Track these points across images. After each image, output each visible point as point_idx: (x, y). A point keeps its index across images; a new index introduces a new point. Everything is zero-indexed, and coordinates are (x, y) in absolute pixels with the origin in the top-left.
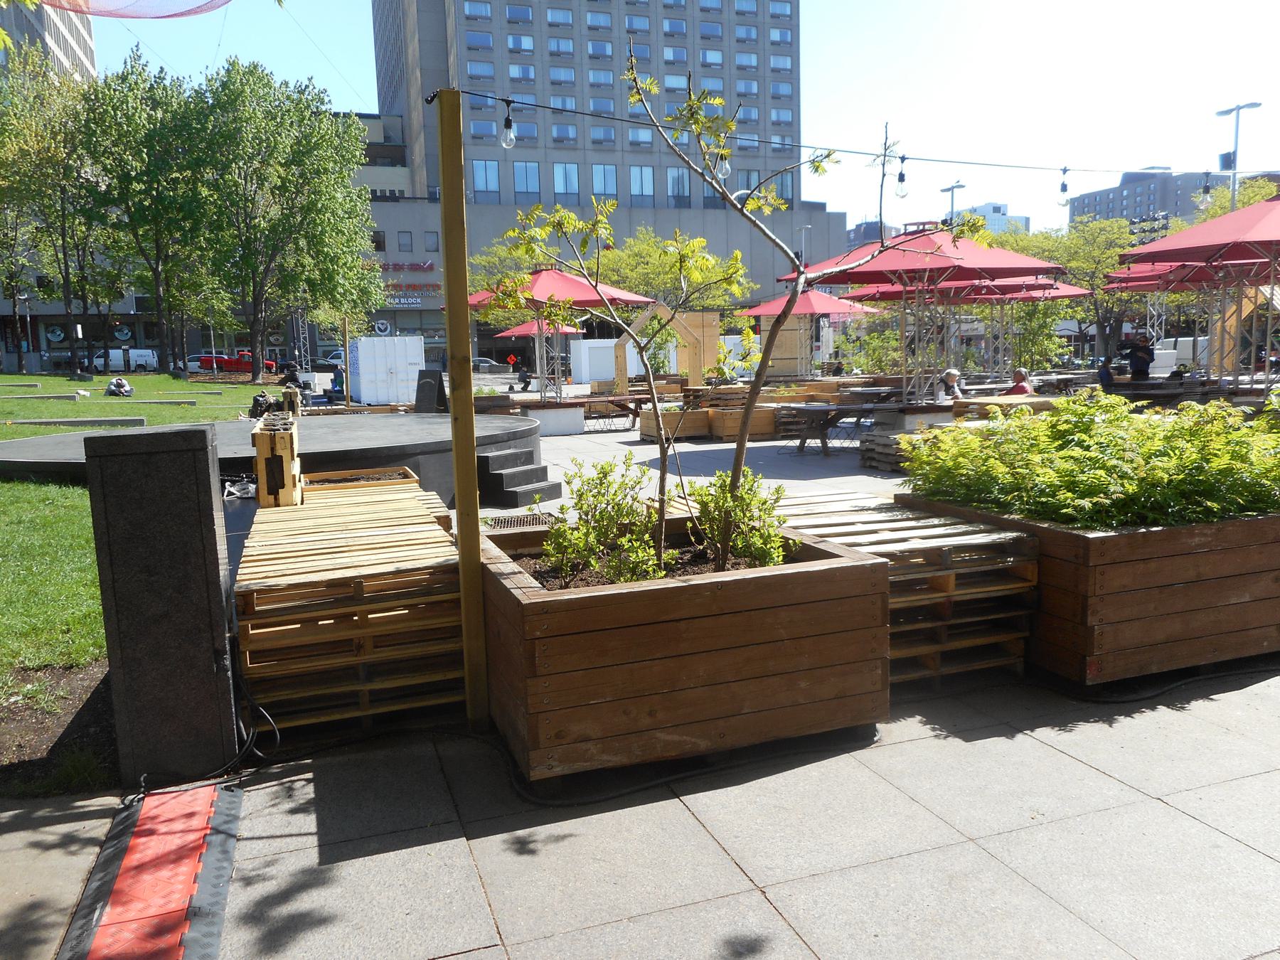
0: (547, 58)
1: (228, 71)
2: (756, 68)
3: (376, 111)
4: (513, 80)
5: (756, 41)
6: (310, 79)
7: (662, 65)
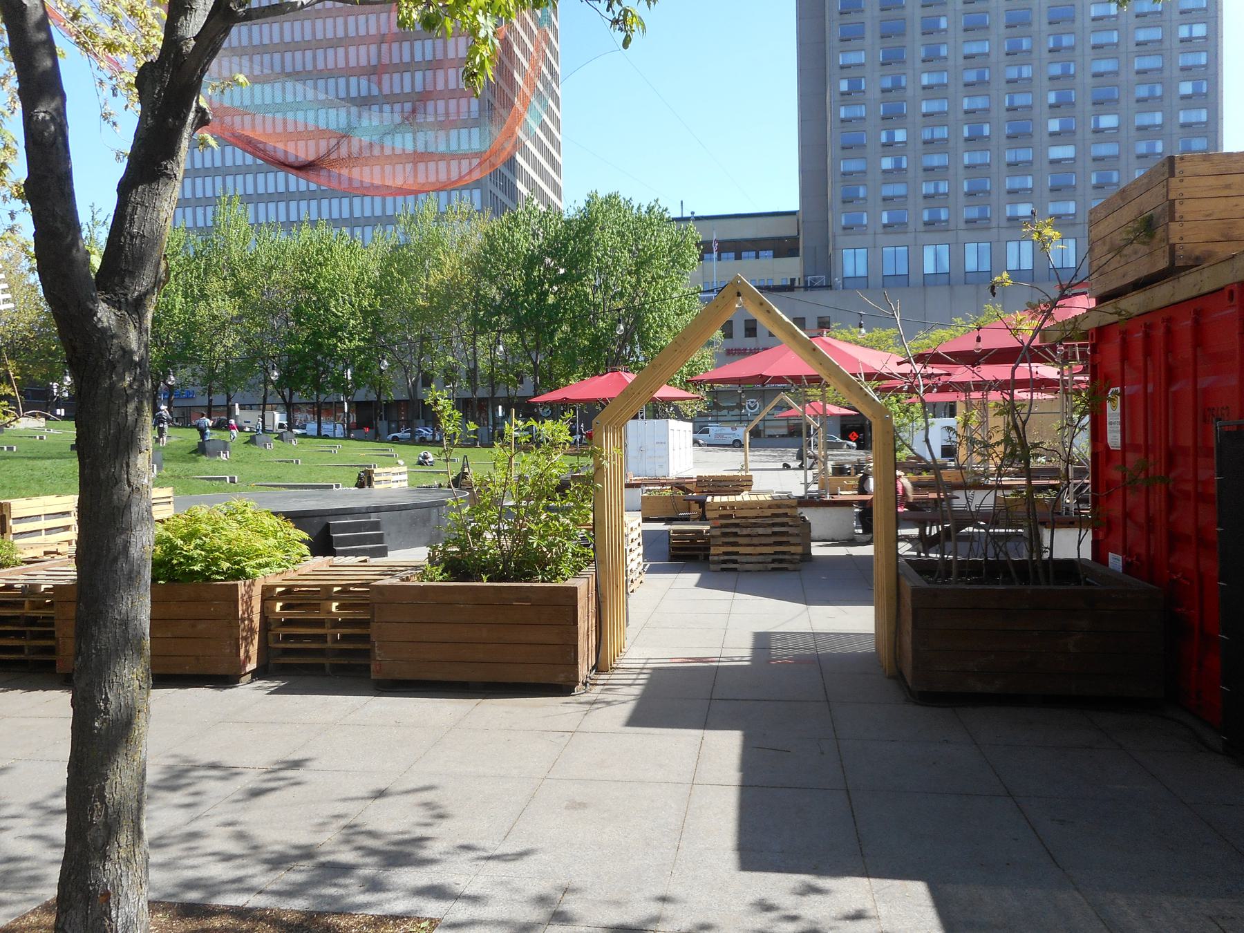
0: (920, 146)
1: (588, 202)
4: (885, 171)
6: (656, 201)
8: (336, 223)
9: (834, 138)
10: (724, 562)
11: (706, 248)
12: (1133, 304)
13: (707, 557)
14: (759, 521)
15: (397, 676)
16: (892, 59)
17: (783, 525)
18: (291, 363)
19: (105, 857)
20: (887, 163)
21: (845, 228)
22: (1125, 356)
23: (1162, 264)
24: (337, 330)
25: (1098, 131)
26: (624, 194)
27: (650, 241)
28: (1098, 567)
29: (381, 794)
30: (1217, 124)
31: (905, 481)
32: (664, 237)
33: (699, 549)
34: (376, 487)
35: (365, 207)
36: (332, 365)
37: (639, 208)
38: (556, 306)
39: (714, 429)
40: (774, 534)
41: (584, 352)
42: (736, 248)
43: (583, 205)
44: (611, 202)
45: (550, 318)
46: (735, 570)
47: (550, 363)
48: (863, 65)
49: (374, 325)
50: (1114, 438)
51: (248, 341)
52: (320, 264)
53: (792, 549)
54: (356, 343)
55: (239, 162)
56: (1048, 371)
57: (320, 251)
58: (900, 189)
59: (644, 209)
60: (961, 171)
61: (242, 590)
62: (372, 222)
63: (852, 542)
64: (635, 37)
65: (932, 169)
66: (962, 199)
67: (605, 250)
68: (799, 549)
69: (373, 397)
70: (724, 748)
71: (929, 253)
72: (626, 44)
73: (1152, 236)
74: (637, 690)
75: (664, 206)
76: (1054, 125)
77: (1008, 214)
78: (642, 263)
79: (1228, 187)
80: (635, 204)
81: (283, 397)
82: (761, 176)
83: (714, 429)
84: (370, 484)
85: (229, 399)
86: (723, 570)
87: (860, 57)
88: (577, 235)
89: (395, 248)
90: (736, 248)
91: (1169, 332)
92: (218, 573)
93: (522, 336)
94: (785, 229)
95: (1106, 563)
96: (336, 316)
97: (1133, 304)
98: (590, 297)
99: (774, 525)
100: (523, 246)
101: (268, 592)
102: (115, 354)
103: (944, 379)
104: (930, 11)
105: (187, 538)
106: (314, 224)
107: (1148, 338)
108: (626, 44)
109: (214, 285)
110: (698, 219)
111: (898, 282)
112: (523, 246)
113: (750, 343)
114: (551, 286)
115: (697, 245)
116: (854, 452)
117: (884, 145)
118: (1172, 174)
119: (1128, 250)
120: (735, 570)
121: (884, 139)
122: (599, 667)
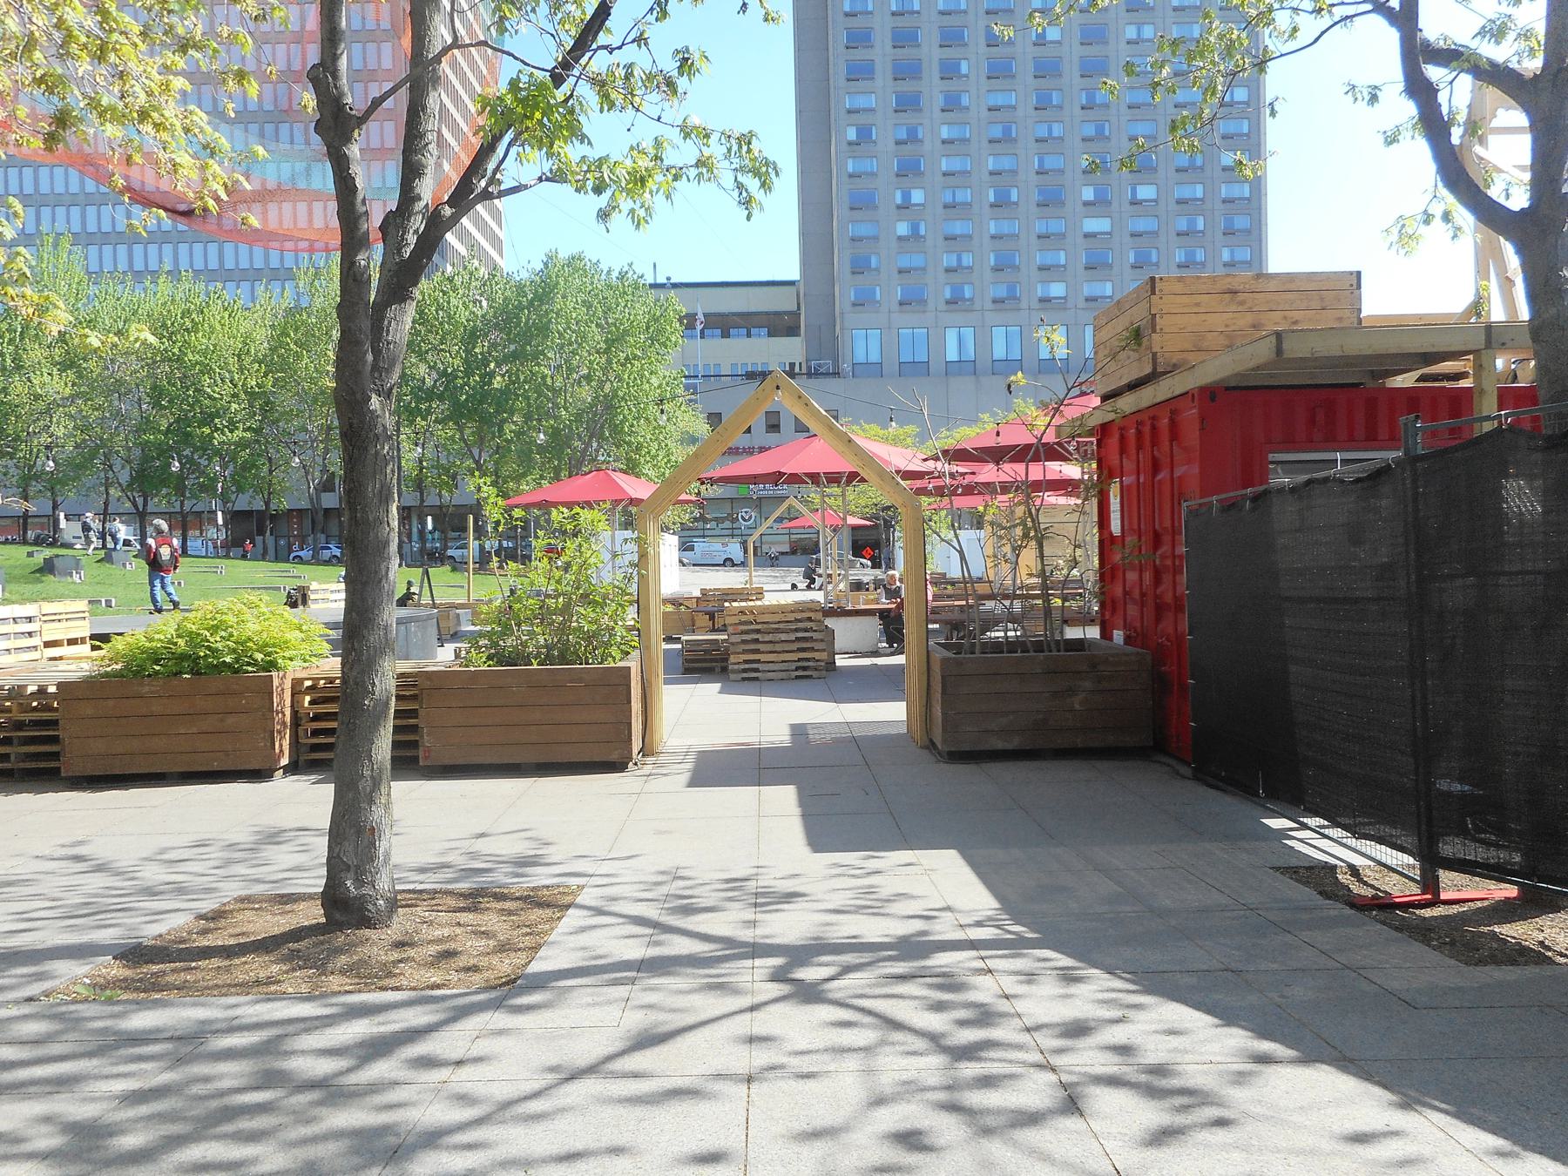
0: (940, 210)
1: (546, 265)
2: (1201, 200)
3: (794, 275)
4: (900, 238)
5: (1202, 168)
6: (630, 265)
7: (1080, 208)
8: (210, 275)
9: (840, 194)
10: (745, 671)
11: (689, 321)
12: (1127, 403)
13: (724, 670)
14: (781, 626)
15: (447, 762)
16: (907, 104)
17: (806, 630)
18: (146, 459)
19: (371, 801)
20: (902, 229)
21: (854, 305)
22: (1123, 451)
23: (1148, 370)
24: (212, 416)
25: (1135, 202)
26: (591, 255)
27: (629, 317)
28: (1105, 642)
29: (482, 835)
30: (1260, 199)
31: (931, 591)
32: (640, 309)
33: (715, 661)
34: (313, 606)
35: (238, 255)
36: (204, 462)
37: (609, 272)
38: (505, 392)
39: (700, 546)
40: (798, 639)
41: (542, 449)
42: (722, 324)
43: (540, 266)
44: (575, 262)
45: (499, 404)
46: (756, 679)
47: (496, 463)
48: (872, 110)
49: (264, 412)
50: (1116, 526)
51: (84, 429)
52: (187, 330)
53: (817, 655)
54: (238, 434)
55: (74, 188)
56: (1072, 471)
57: (186, 313)
58: (917, 260)
59: (615, 274)
60: (986, 240)
61: (276, 682)
62: (251, 276)
63: (876, 653)
64: (755, 212)
65: (954, 238)
66: (988, 275)
67: (568, 323)
68: (824, 656)
69: (259, 505)
70: (784, 797)
71: (951, 337)
72: (748, 218)
73: (1140, 345)
74: (689, 766)
75: (639, 272)
76: (1088, 194)
77: (1039, 294)
78: (614, 341)
79: (1198, 305)
80: (604, 267)
81: (135, 504)
82: (763, 246)
83: (700, 546)
84: (305, 603)
85: (55, 507)
86: (744, 679)
87: (871, 101)
88: (531, 303)
89: (289, 312)
90: (722, 324)
91: (1154, 428)
92: (249, 664)
93: (461, 429)
94: (783, 302)
95: (1111, 639)
96: (210, 397)
97: (1127, 403)
98: (549, 381)
99: (796, 630)
100: (463, 316)
101: (297, 683)
102: (380, 430)
103: (968, 479)
104: (948, 53)
105: (214, 629)
106: (175, 274)
107: (1139, 433)
108: (748, 218)
109: (35, 354)
110: (675, 286)
111: (915, 370)
112: (463, 316)
113: (772, 438)
114: (498, 365)
115: (680, 320)
116: (869, 571)
117: (899, 207)
118: (1153, 293)
119: (1122, 355)
120: (756, 679)
121: (899, 200)
122: (646, 751)
